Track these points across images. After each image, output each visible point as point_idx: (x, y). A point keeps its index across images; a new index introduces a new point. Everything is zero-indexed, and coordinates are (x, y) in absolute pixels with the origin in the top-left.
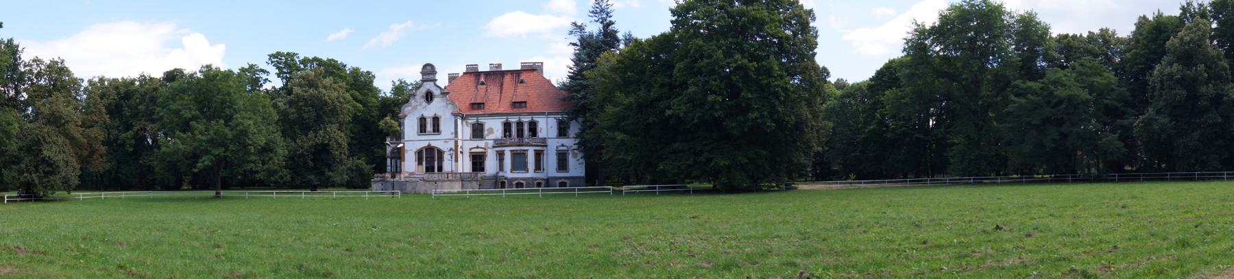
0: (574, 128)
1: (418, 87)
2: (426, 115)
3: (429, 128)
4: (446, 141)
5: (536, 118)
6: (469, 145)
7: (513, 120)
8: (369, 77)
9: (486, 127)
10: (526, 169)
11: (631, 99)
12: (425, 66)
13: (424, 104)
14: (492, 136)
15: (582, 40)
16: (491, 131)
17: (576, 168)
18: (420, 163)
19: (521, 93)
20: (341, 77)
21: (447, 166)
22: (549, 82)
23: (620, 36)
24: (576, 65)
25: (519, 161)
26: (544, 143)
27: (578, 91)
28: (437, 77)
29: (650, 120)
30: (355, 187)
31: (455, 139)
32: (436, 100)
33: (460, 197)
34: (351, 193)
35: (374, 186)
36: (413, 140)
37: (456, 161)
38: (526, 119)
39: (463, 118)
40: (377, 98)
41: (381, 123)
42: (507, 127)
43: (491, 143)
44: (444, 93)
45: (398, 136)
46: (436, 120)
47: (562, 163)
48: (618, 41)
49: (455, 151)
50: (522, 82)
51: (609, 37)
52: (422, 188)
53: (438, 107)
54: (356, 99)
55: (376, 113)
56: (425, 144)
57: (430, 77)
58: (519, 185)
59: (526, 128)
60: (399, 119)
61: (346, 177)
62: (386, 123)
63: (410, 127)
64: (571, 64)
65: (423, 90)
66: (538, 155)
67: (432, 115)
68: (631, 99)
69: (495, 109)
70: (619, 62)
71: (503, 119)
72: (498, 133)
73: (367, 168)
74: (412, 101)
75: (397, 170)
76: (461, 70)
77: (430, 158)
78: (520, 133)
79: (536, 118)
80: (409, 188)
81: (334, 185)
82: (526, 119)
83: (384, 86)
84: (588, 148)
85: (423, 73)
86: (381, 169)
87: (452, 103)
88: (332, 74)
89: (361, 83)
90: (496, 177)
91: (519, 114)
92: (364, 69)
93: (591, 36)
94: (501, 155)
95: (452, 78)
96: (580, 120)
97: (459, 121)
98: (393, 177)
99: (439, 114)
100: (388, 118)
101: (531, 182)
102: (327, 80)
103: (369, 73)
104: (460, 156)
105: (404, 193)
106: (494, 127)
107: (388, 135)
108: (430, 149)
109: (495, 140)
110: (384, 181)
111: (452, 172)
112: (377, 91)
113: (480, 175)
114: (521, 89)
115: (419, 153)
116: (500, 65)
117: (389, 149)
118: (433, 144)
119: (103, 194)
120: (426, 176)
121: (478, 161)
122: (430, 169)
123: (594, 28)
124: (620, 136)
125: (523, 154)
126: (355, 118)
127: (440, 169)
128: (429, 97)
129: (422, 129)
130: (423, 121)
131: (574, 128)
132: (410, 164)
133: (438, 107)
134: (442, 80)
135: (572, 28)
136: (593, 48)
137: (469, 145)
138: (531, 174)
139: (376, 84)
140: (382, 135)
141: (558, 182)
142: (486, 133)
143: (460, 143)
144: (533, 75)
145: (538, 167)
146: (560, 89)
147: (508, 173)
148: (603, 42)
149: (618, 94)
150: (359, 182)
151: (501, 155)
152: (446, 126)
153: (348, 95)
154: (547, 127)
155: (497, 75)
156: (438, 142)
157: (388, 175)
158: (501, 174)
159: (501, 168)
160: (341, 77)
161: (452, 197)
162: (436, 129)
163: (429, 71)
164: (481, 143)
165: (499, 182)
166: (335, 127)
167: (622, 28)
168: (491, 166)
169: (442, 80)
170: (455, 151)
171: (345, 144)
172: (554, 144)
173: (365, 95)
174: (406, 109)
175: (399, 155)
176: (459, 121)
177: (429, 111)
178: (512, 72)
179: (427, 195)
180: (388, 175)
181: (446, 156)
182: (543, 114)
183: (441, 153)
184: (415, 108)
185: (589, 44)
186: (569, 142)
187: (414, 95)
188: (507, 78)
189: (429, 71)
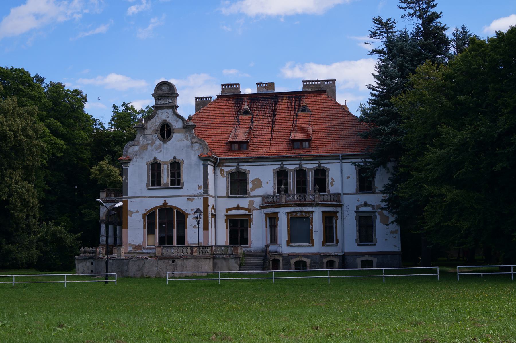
0: (381, 179)
1: (150, 115)
3: (165, 178)
4: (190, 198)
5: (325, 165)
6: (224, 204)
7: (291, 167)
8: (78, 98)
9: (251, 177)
10: (309, 240)
11: (466, 134)
13: (158, 142)
14: (259, 192)
15: (390, 43)
16: (258, 183)
17: (387, 238)
18: (150, 231)
19: (303, 127)
20: (32, 98)
21: (192, 236)
22: (344, 108)
23: (449, 34)
24: (382, 83)
25: (300, 229)
26: (337, 201)
27: (386, 123)
28: (179, 101)
29: (498, 168)
30: (50, 268)
31: (204, 195)
32: (176, 137)
33: (209, 283)
34: (41, 278)
35: (80, 266)
36: (140, 197)
37: (206, 228)
38: (310, 166)
39: (217, 164)
40: (89, 131)
41: (94, 170)
42: (282, 176)
43: (258, 202)
44: (188, 126)
45: (119, 189)
46: (176, 166)
47: (366, 232)
48: (447, 42)
49: (205, 214)
50: (304, 110)
51: (431, 35)
52: (152, 268)
53: (178, 147)
54: (55, 132)
55: (87, 155)
56: (159, 202)
57: (168, 101)
58: (300, 264)
59: (310, 178)
60: (122, 165)
61: (35, 252)
62: (101, 170)
63: (136, 177)
64: (374, 82)
65: (156, 122)
66: (329, 220)
68: (466, 134)
69: (263, 151)
70: (448, 77)
71: (277, 167)
72: (269, 187)
73: (69, 239)
74: (140, 139)
75: (118, 242)
76: (214, 92)
77: (166, 223)
78: (301, 186)
80: (133, 269)
81: (15, 266)
82: (310, 166)
83: (100, 111)
84: (404, 209)
85: (156, 96)
86: (91, 239)
87: (201, 141)
88: (18, 92)
89: (65, 106)
90: (264, 253)
91: (300, 158)
92: (70, 86)
93: (404, 37)
94: (272, 221)
95: (202, 103)
96: (390, 165)
97: (210, 169)
98: (109, 252)
99: (180, 157)
100: (104, 163)
101: (317, 260)
102: (8, 100)
103: (77, 92)
104: (211, 221)
105: (124, 276)
106: (263, 178)
107: (103, 187)
108: (166, 211)
109: (264, 197)
110: (94, 258)
111: (199, 245)
112: (89, 120)
113: (241, 249)
114: (303, 121)
115: (150, 216)
116: (271, 85)
117: (103, 211)
118: (171, 202)
120: (159, 251)
121: (238, 227)
122: (165, 241)
123: (408, 25)
124: (451, 194)
125: (307, 218)
126: (54, 162)
127: (181, 240)
128: (165, 132)
129: (155, 180)
130: (155, 168)
131: (381, 179)
132: (135, 233)
133: (178, 147)
134: (186, 106)
135: (373, 27)
136: (406, 58)
137: (224, 204)
138: (317, 248)
139: (88, 108)
140: (95, 187)
141: (359, 260)
142: (251, 186)
143: (211, 202)
144: (320, 99)
145: (329, 237)
146: (361, 120)
147: (284, 248)
148: (423, 46)
149: (444, 129)
150: (57, 260)
151: (272, 221)
152: (192, 178)
153: (41, 126)
154: (341, 176)
155: (267, 98)
156: (177, 200)
157: (101, 250)
158: (272, 248)
159: (273, 239)
160: (32, 98)
161: (196, 284)
162: (176, 180)
163: (165, 93)
164: (244, 202)
165: (269, 260)
166: (17, 175)
167: (451, 25)
168: (257, 236)
169: (186, 106)
170: (205, 214)
171: (35, 201)
172: (352, 203)
173: (70, 126)
174: (132, 149)
175: (119, 218)
176: (210, 169)
177: (165, 153)
178: (289, 95)
179: (160, 278)
180: (101, 250)
181: (191, 221)
182: (335, 157)
183: (182, 216)
184: (144, 147)
185: (401, 50)
186: (374, 200)
187: (143, 129)
188: (283, 104)
189: (165, 93)
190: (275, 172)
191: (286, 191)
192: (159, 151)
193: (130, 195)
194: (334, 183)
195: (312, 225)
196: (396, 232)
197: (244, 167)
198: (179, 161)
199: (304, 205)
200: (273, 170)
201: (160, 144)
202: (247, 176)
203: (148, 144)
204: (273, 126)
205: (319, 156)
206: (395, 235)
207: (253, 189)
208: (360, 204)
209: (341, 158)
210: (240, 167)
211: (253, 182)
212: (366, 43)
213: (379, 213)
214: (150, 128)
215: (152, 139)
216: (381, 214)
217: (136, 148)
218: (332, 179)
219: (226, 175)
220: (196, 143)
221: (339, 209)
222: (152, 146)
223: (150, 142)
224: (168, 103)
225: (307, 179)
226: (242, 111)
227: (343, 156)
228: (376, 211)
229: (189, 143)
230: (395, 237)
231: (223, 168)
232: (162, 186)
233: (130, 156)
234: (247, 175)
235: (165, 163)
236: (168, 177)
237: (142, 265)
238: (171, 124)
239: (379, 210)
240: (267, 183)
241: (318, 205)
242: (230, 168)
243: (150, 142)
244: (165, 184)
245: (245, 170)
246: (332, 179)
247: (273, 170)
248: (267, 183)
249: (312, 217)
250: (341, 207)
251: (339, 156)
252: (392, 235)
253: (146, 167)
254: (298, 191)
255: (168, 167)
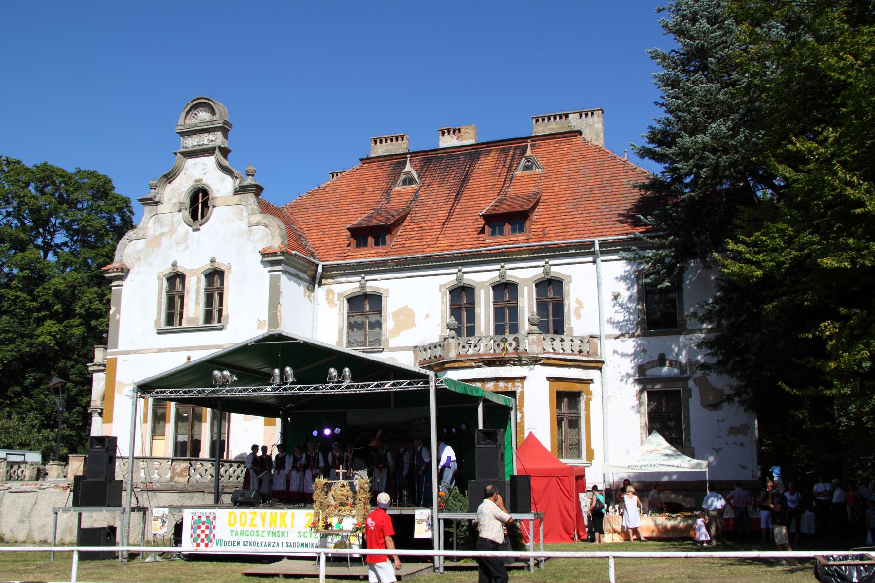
2: (183, 266)
3: (194, 307)
9: (390, 306)
12: (406, 308)
16: (407, 318)
32: (216, 215)
42: (461, 298)
59: (527, 303)
63: (136, 305)
67: (204, 264)
79: (560, 268)
99: (222, 263)
119: (448, 307)
123: (488, 230)
142: (388, 324)
174: (128, 250)
182: (583, 250)
184: (156, 242)
190: (444, 290)
191: (471, 332)
192: (183, 247)
193: (121, 347)
194: (582, 311)
195: (522, 412)
196: (745, 429)
197: (376, 283)
198: (222, 268)
199: (501, 362)
200: (441, 286)
201: (187, 232)
202: (383, 303)
203: (163, 234)
204: (457, 198)
205: (546, 249)
206: (741, 438)
207: (395, 333)
208: (648, 360)
209: (597, 247)
210: (368, 284)
211: (396, 315)
212: (659, 11)
213: (697, 382)
214: (169, 200)
215: (172, 223)
216: (702, 383)
217: (140, 244)
218: (577, 301)
219: (337, 302)
220: (258, 224)
221: (593, 374)
222: (171, 236)
223: (166, 229)
224: (206, 142)
225: (520, 304)
226: (402, 177)
227: (602, 244)
228: (689, 378)
229: (244, 225)
230: (742, 445)
231: (332, 287)
232: (185, 324)
233: (128, 263)
234: (383, 299)
235: (194, 272)
236: (197, 303)
237: (30, 506)
238: (210, 189)
239: (699, 373)
240: (428, 316)
241: (536, 361)
242: (350, 286)
243: (166, 229)
244: (190, 321)
245: (379, 289)
246: (577, 301)
247: (441, 286)
248: (428, 316)
249: (522, 393)
250: (600, 369)
251: (593, 243)
252: (733, 438)
253: (155, 284)
254: (499, 330)
255: (199, 281)
